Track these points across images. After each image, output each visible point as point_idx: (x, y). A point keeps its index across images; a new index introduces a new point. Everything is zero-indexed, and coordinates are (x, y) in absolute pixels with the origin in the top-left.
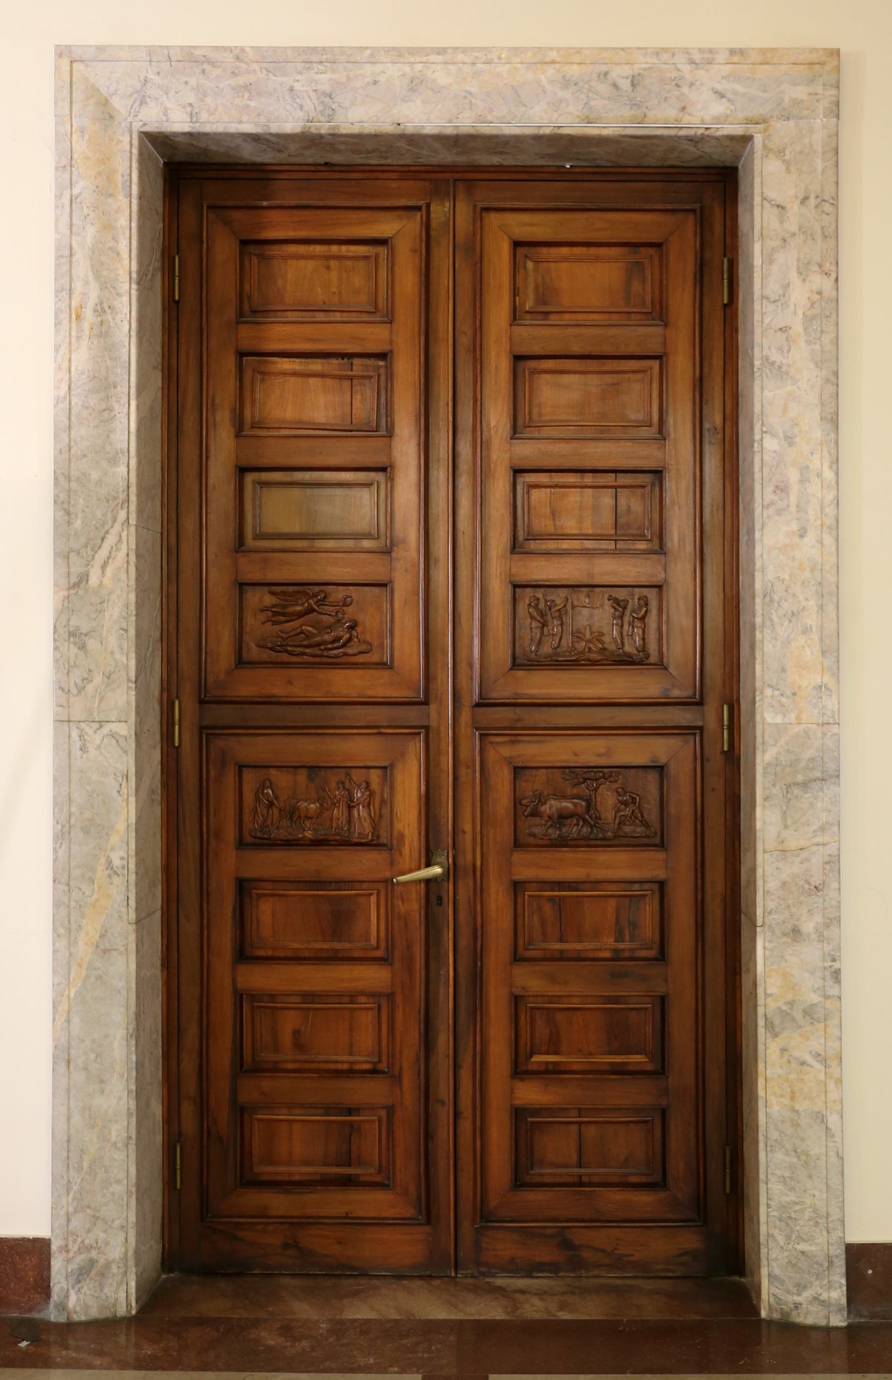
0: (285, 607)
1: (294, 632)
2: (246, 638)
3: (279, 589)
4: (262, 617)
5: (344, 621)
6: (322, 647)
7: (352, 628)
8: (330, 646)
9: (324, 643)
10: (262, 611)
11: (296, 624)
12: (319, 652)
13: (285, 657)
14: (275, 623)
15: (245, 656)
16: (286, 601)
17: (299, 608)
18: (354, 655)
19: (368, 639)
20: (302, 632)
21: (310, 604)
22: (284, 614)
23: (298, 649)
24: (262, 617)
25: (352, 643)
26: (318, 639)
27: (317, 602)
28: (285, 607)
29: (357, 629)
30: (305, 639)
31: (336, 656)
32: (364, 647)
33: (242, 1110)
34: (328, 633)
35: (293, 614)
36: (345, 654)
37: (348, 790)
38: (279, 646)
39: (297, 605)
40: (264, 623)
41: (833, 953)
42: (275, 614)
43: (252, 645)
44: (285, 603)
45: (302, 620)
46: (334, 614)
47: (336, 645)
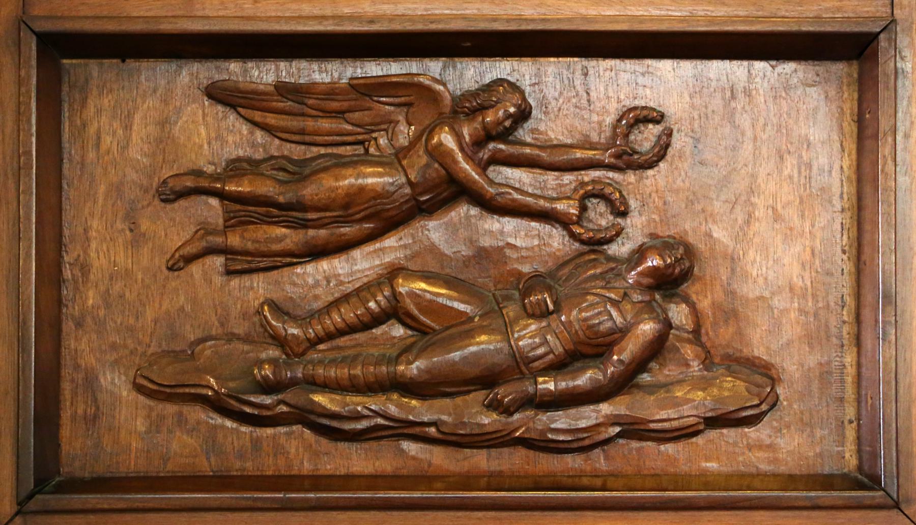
0: (299, 172)
1: (348, 314)
2: (81, 347)
3: (265, 74)
4: (175, 227)
5: (620, 249)
6: (506, 393)
7: (668, 283)
8: (548, 384)
9: (520, 366)
10: (172, 195)
11: (360, 265)
12: (488, 419)
13: (298, 450)
14: (242, 263)
15: (74, 444)
16: (303, 137)
17: (374, 179)
18: (684, 434)
19: (759, 345)
20: (394, 312)
21: (438, 154)
22: (292, 212)
23: (374, 403)
24: (175, 227)
25: (670, 372)
26: (484, 344)
27: (479, 143)
28: (299, 172)
29: (691, 289)
30: (406, 351)
31: (582, 444)
32: (731, 390)
33: (353, 386)
34: (542, 314)
35: (349, 206)
36: (634, 430)
37: (303, 354)
38: (267, 387)
39: (365, 160)
40: (180, 262)
41: (89, 320)
42: (245, 209)
43: (115, 383)
44: (297, 152)
45: (394, 247)
46: (569, 207)
47: (584, 379)
